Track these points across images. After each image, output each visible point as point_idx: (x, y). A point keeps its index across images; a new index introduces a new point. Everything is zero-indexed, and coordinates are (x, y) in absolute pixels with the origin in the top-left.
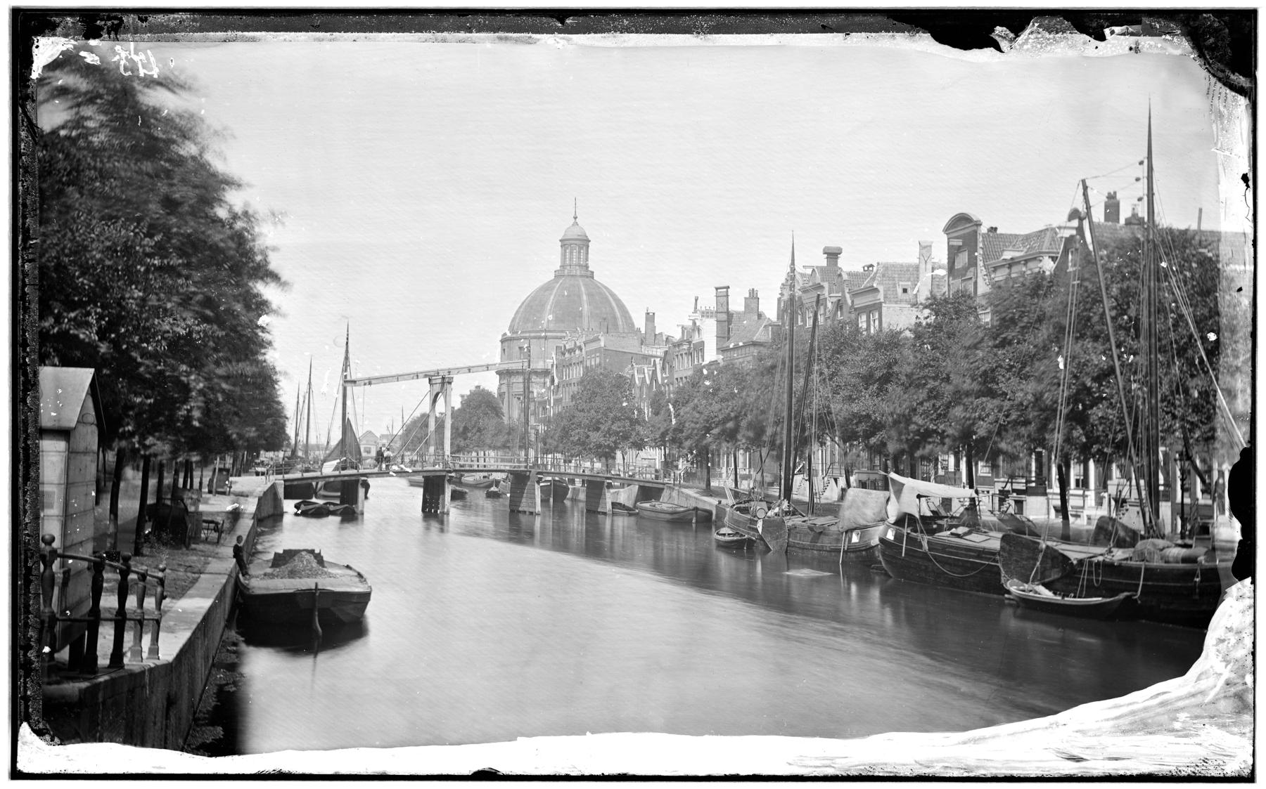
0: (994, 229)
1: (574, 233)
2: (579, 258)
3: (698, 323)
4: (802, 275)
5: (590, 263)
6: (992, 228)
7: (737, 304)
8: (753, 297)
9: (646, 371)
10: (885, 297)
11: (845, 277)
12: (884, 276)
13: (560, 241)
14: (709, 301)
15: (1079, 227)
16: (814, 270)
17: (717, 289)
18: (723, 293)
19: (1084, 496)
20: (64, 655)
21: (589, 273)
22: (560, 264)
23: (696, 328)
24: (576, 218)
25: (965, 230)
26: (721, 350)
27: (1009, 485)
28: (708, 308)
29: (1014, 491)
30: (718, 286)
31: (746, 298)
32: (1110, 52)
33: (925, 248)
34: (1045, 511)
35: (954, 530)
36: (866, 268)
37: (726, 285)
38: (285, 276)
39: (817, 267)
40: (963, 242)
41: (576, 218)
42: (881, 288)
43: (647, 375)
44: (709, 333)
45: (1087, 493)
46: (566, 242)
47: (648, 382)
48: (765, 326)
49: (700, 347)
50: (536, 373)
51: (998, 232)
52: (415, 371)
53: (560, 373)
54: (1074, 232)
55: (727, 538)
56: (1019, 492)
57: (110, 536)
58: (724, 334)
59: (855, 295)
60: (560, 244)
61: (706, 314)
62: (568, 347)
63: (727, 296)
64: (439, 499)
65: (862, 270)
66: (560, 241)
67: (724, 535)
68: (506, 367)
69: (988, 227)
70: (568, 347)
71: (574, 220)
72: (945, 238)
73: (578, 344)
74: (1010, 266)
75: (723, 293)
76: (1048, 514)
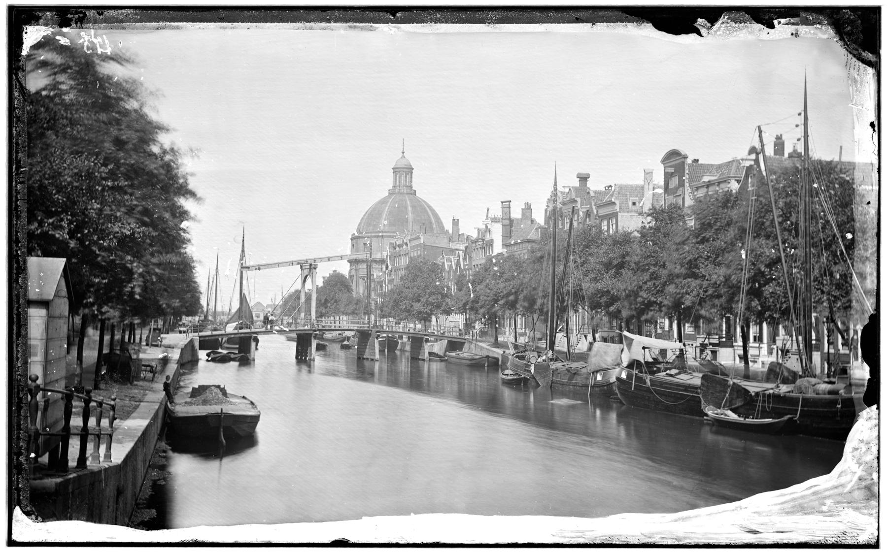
0: (696, 161)
1: (402, 163)
2: (406, 181)
3: (489, 227)
4: (562, 193)
5: (413, 184)
6: (695, 160)
7: (516, 213)
8: (528, 208)
9: (453, 260)
10: (620, 208)
11: (592, 194)
12: (619, 193)
13: (393, 169)
14: (497, 211)
15: (756, 159)
16: (570, 189)
17: (502, 202)
18: (506, 205)
19: (759, 348)
20: (45, 459)
21: (413, 192)
22: (392, 185)
23: (488, 230)
24: (403, 153)
25: (676, 161)
26: (505, 245)
27: (707, 340)
28: (496, 216)
29: (710, 344)
30: (503, 200)
31: (522, 209)
32: (778, 37)
33: (648, 174)
34: (732, 358)
35: (668, 372)
36: (607, 188)
37: (508, 200)
38: (199, 194)
39: (572, 187)
40: (675, 170)
41: (403, 153)
42: (617, 202)
43: (453, 263)
44: (497, 233)
45: (761, 345)
46: (396, 170)
47: (454, 268)
48: (536, 229)
49: (491, 243)
50: (375, 261)
51: (700, 162)
52: (291, 260)
53: (392, 261)
54: (752, 163)
55: (510, 377)
56: (714, 345)
57: (77, 376)
58: (508, 234)
59: (599, 207)
60: (392, 171)
61: (495, 220)
62: (398, 243)
63: (510, 207)
64: (307, 350)
65: (604, 189)
66: (393, 169)
67: (507, 375)
68: (354, 257)
69: (693, 159)
70: (398, 243)
71: (402, 154)
72: (662, 166)
73: (405, 241)
74: (708, 187)
75: (506, 205)
76: (735, 360)
